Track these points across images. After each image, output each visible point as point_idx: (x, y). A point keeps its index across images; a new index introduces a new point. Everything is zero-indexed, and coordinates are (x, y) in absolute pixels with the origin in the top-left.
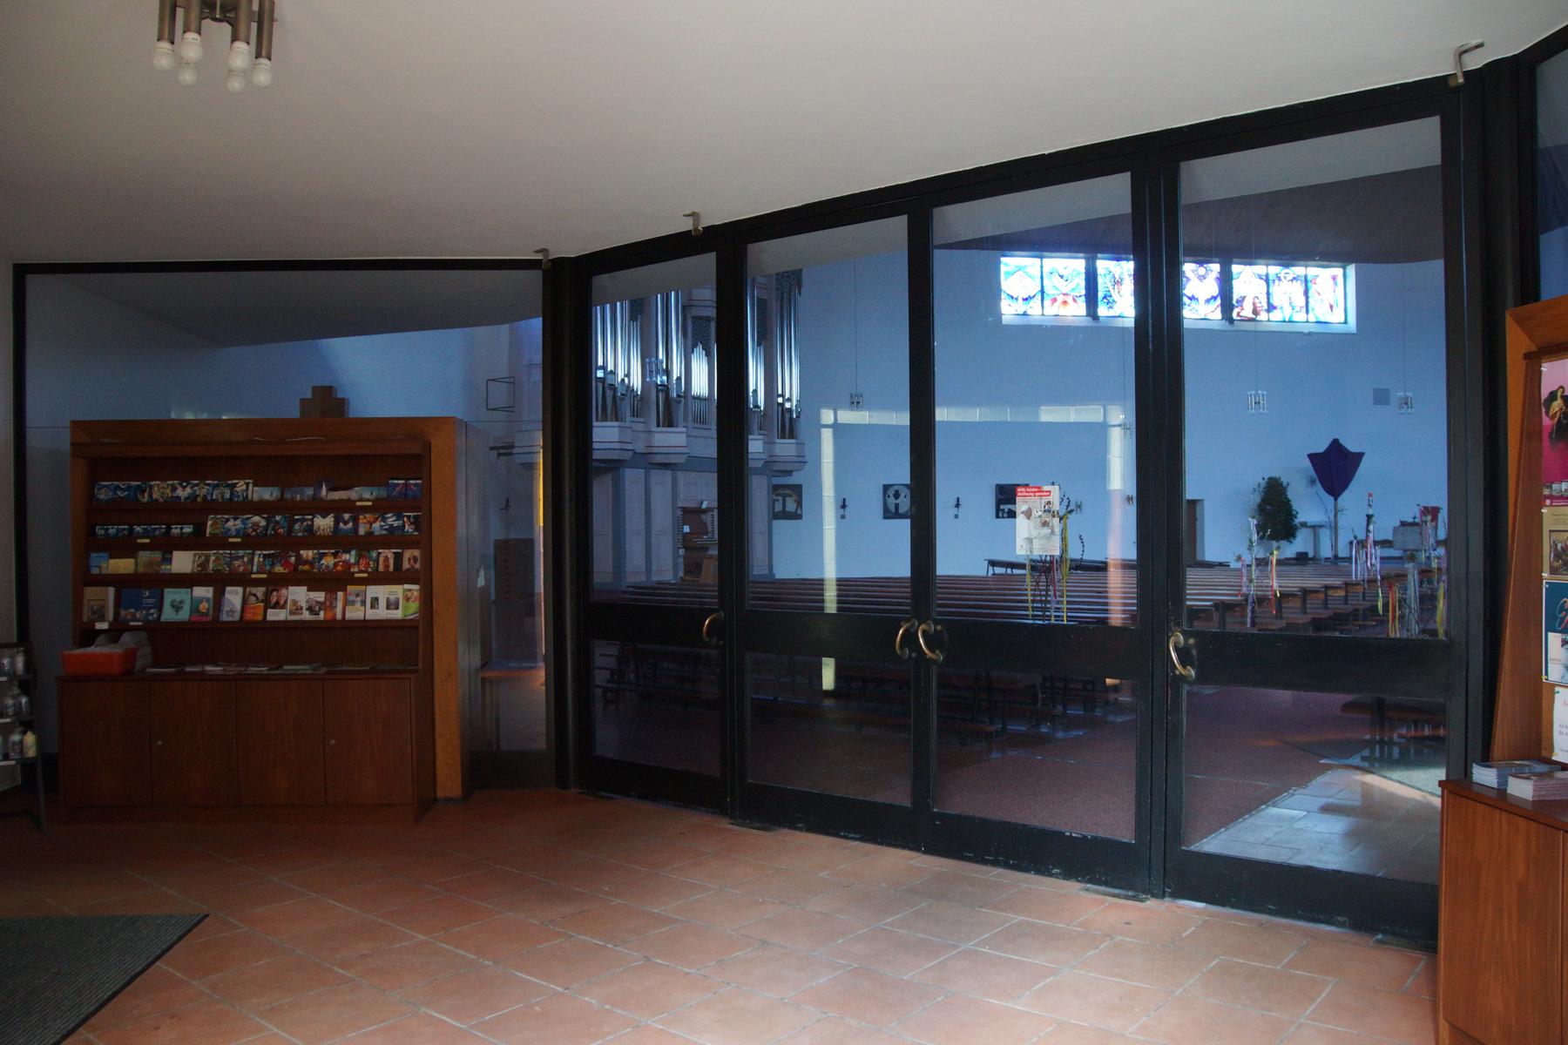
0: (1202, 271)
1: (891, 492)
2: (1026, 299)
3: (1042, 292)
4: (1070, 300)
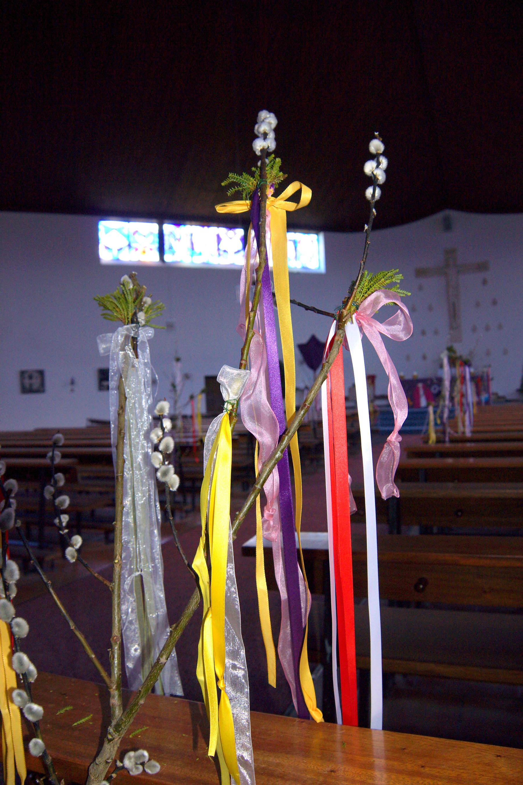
0: (231, 232)
1: (26, 375)
2: (119, 250)
3: (129, 246)
4: (147, 250)
